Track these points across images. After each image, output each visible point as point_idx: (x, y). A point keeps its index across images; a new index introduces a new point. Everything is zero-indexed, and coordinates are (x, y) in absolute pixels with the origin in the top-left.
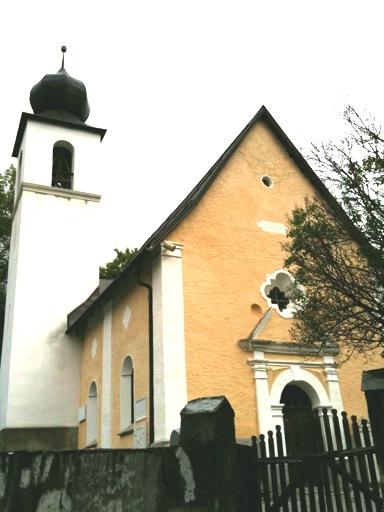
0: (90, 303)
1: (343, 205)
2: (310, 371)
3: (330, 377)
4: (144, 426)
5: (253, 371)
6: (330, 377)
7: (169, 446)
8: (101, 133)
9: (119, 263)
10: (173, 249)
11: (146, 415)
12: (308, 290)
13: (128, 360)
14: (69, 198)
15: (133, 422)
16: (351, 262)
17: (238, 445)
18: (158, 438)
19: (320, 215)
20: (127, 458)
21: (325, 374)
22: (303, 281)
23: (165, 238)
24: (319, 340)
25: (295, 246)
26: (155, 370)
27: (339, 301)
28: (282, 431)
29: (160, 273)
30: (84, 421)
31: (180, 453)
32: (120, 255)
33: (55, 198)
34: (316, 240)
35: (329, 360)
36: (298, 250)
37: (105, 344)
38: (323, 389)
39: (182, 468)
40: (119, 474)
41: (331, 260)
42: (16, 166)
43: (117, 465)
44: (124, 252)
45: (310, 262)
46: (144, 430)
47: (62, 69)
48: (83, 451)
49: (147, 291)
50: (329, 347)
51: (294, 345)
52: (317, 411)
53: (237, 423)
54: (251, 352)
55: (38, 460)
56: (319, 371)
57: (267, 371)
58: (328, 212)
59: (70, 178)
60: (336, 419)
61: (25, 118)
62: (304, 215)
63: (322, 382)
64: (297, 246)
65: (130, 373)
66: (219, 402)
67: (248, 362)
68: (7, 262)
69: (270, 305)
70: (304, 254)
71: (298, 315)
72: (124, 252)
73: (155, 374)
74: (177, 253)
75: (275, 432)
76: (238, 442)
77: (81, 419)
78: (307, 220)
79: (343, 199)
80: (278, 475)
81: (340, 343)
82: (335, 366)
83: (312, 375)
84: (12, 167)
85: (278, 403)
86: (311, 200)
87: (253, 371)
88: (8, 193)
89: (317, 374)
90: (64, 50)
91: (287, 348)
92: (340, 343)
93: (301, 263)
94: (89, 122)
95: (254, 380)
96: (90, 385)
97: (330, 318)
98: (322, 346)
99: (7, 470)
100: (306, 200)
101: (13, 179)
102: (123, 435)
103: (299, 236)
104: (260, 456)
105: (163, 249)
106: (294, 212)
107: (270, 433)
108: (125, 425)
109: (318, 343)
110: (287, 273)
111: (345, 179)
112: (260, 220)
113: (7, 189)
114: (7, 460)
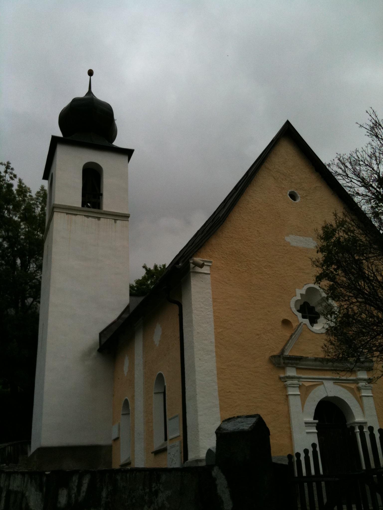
0: (121, 321)
1: (372, 220)
2: (343, 386)
3: (364, 393)
4: (178, 444)
5: (286, 387)
6: (364, 393)
7: (203, 464)
8: (128, 153)
9: (148, 280)
10: (202, 266)
11: (179, 433)
12: (341, 306)
13: (160, 378)
14: (99, 218)
15: (166, 439)
16: (245, 270)
17: (275, 464)
18: (191, 456)
19: (349, 230)
20: (164, 477)
21: (359, 389)
22: (335, 297)
23: (193, 256)
24: (353, 356)
25: (325, 261)
26: (187, 387)
27: (372, 316)
28: (318, 449)
29: (190, 290)
30: (117, 439)
31: (216, 472)
32: (148, 271)
33: (86, 218)
34: (346, 255)
35: (363, 375)
36: (328, 266)
37: (136, 362)
38: (358, 405)
39: (218, 487)
40: (156, 493)
41: (362, 275)
42: (46, 188)
43: (154, 485)
44: (152, 268)
45: (342, 278)
46: (178, 448)
47: (90, 92)
48: (117, 471)
49: (176, 307)
50: (363, 362)
51: (328, 360)
52: (353, 428)
53: (272, 441)
54: (282, 368)
55: (75, 479)
56: (353, 386)
57: (300, 387)
58: (359, 227)
59: (99, 198)
60: (372, 436)
61: (55, 141)
62: (334, 230)
63: (356, 398)
64: (328, 261)
65: (163, 391)
66: (254, 420)
67: (280, 378)
68: (40, 283)
69: (301, 320)
70: (335, 270)
71: (330, 331)
72: (152, 268)
73: (187, 391)
74: (205, 270)
75: (311, 450)
76: (274, 460)
77: (115, 436)
78: (337, 235)
79: (373, 213)
80: (315, 493)
81: (374, 359)
82: (369, 381)
83: (346, 391)
84: (42, 188)
85: (311, 419)
86: (340, 215)
87: (286, 387)
88: (39, 215)
89: (351, 390)
90: (91, 73)
91: (318, 363)
92: (374, 359)
93: (332, 279)
94: (118, 143)
95: (287, 396)
96: (122, 403)
97: (363, 334)
98: (356, 362)
99: (44, 489)
100: (335, 215)
101: (44, 201)
102: (157, 453)
103: (330, 252)
104: (296, 475)
105: (192, 265)
106: (323, 228)
107: (306, 451)
108: (158, 443)
109: (351, 360)
110: (318, 288)
111: (373, 194)
112: (288, 235)
113: (38, 210)
114: (45, 479)
